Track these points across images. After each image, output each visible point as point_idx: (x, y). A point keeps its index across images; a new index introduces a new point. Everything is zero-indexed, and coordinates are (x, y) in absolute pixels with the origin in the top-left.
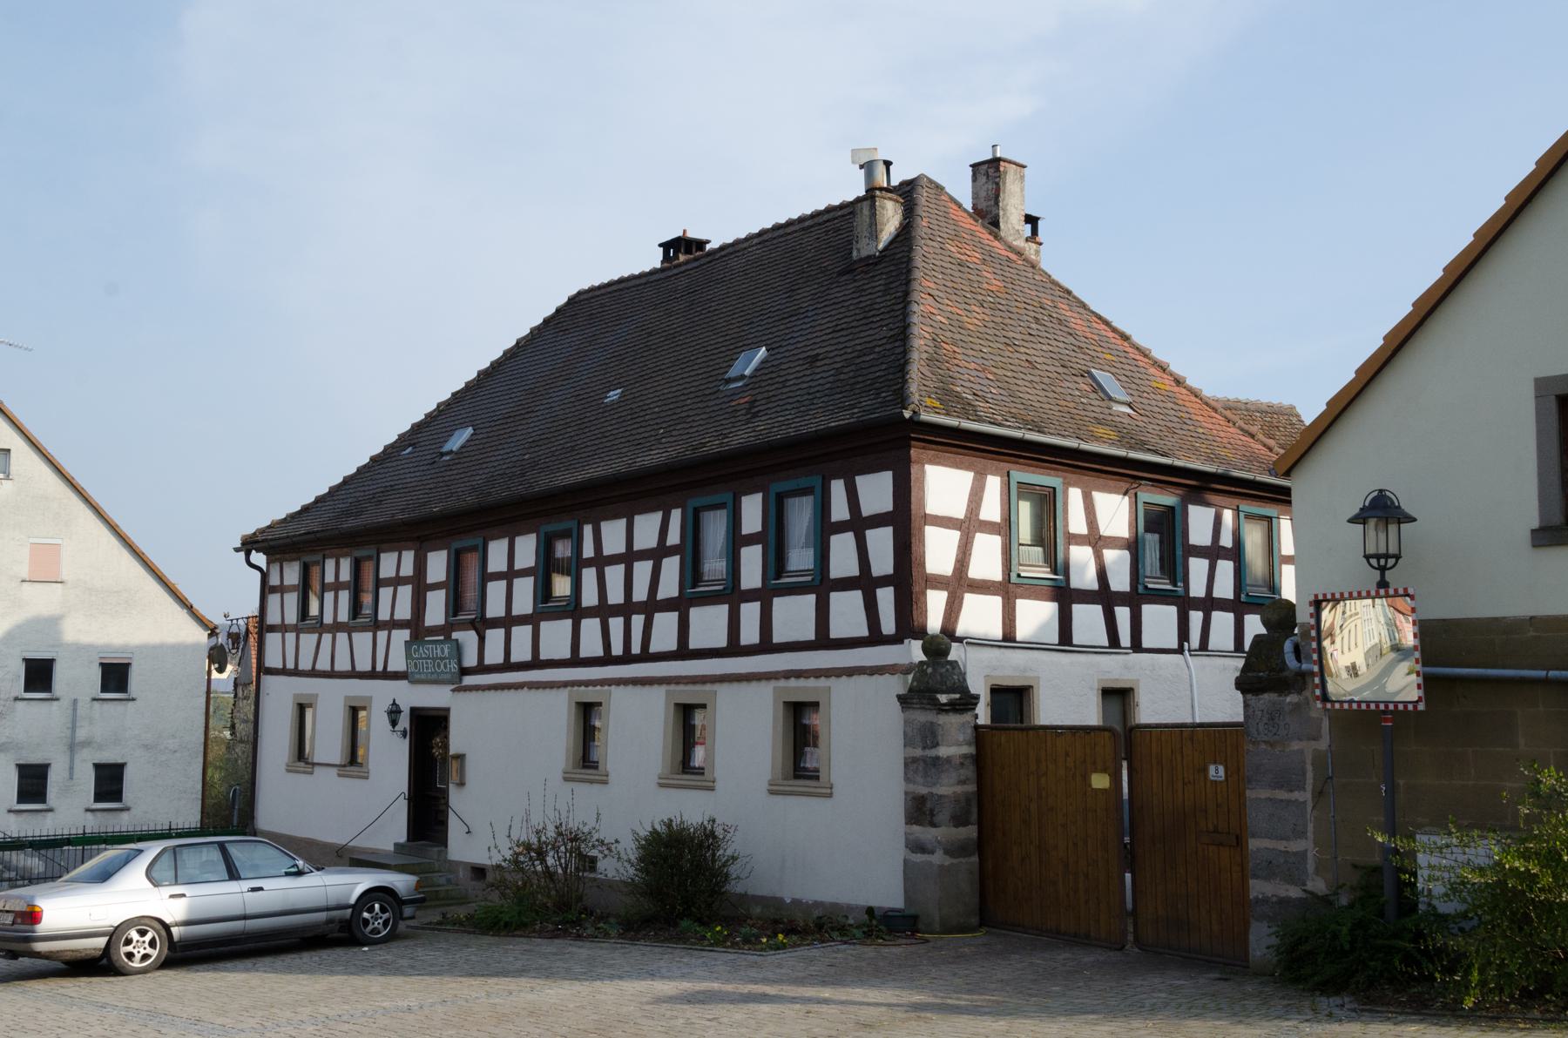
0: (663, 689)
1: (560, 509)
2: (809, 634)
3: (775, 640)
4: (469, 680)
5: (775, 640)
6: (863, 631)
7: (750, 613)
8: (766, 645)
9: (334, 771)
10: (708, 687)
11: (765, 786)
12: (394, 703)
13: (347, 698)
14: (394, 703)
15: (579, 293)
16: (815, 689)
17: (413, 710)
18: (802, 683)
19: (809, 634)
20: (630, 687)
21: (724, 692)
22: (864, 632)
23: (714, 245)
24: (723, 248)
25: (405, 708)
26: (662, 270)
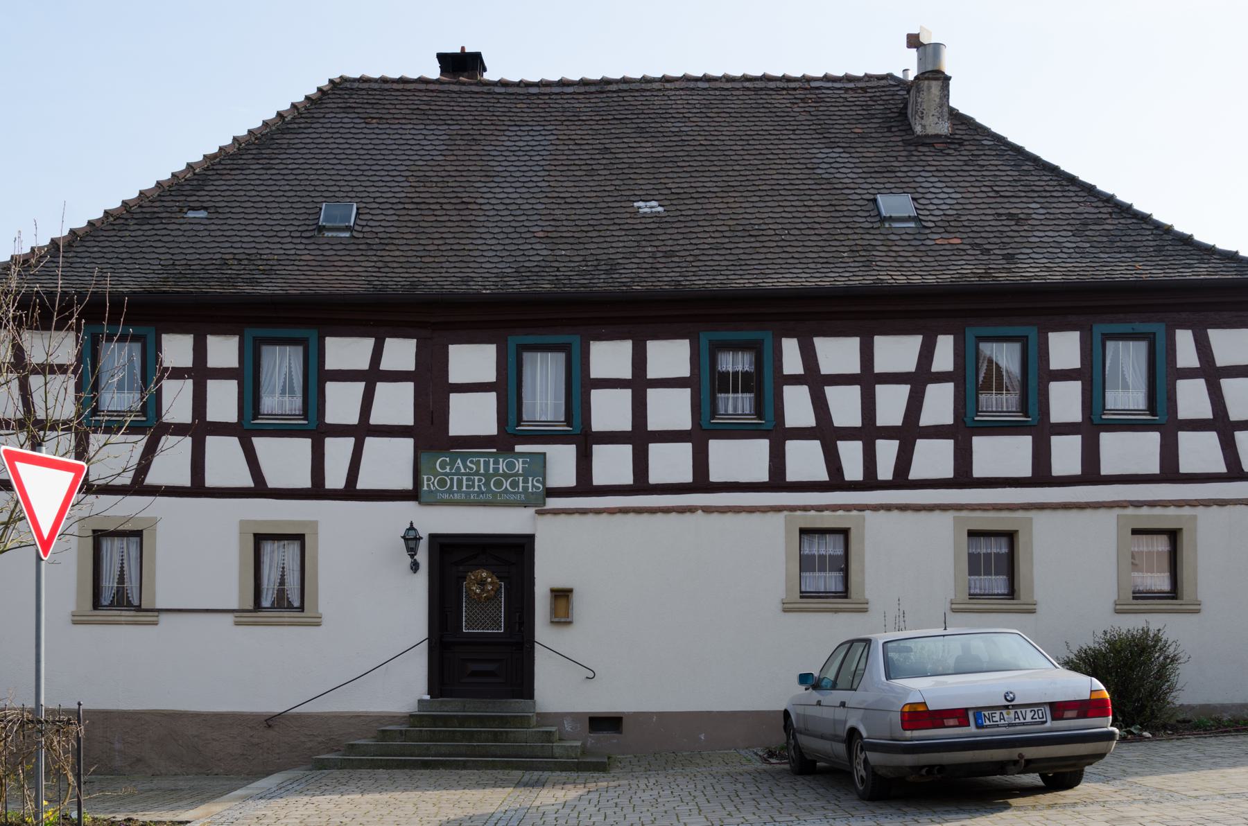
0: (950, 515)
1: (150, 314)
2: (687, 477)
3: (1103, 473)
4: (553, 503)
5: (1103, 473)
6: (305, 482)
7: (338, 451)
8: (901, 480)
9: (230, 618)
10: (1186, 511)
11: (1112, 606)
12: (412, 528)
13: (243, 523)
14: (412, 528)
15: (972, 119)
16: (1178, 517)
17: (432, 537)
18: (1158, 511)
19: (687, 477)
20: (882, 512)
21: (1040, 519)
22: (186, 481)
23: (490, 75)
24: (503, 84)
25: (424, 532)
26: (437, 81)
